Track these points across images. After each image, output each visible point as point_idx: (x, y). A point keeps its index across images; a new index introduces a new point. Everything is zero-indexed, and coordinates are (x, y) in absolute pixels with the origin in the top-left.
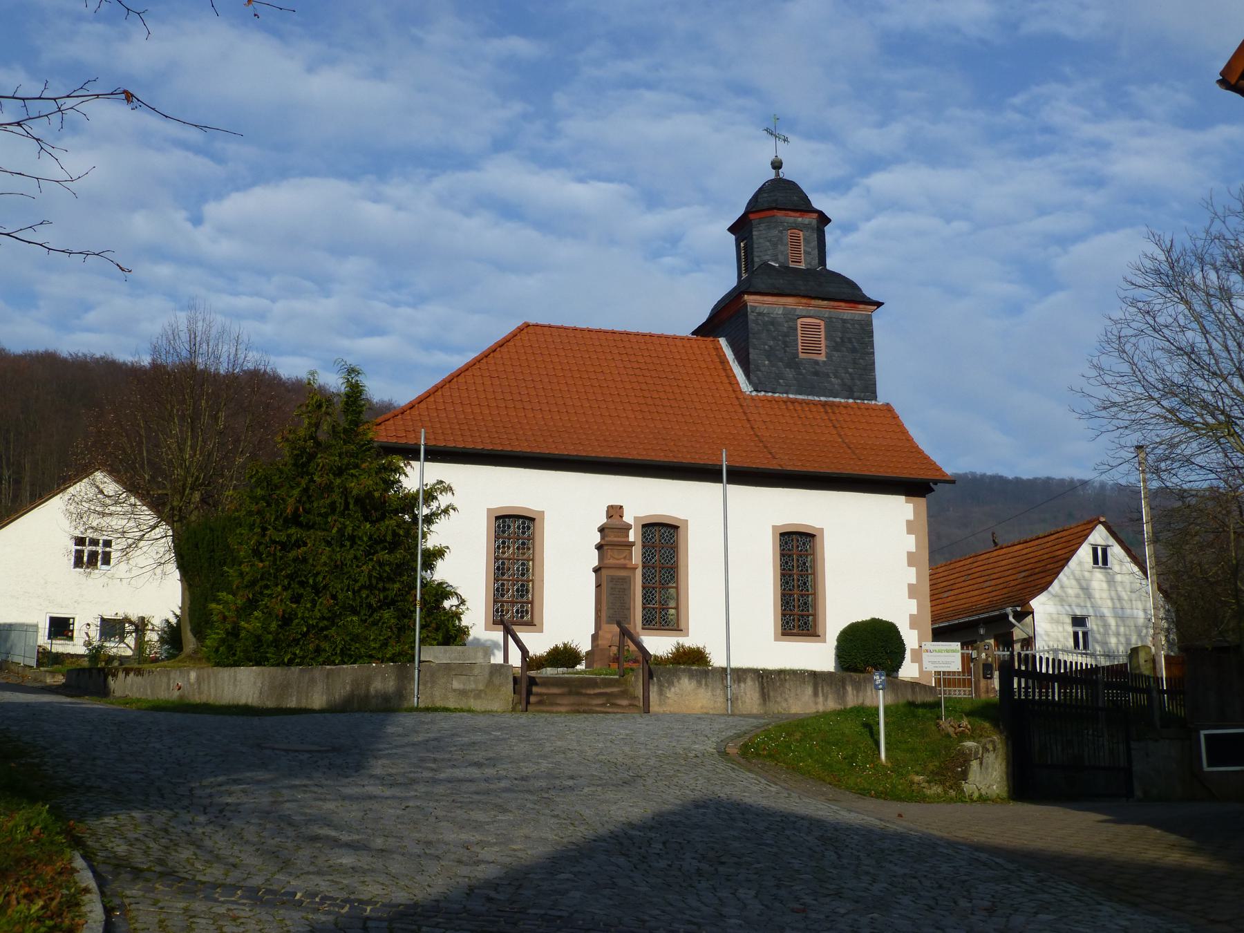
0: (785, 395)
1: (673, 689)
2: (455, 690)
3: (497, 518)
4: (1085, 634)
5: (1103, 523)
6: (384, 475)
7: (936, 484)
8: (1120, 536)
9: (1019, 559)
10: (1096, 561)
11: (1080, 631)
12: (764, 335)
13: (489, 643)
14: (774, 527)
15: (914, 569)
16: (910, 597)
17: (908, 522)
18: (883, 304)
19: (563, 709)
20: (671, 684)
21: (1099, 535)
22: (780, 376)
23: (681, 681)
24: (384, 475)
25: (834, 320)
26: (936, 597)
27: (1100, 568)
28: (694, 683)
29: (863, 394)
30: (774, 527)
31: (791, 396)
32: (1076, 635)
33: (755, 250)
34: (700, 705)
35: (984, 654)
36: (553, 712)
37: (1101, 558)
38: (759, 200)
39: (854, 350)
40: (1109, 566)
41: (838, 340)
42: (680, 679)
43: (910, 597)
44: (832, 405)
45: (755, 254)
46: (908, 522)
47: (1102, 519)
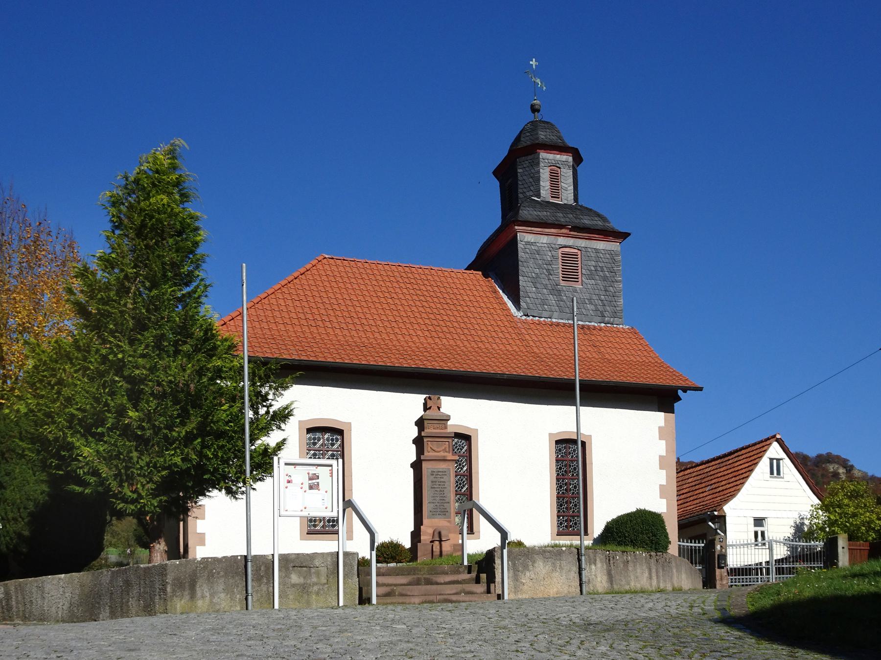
0: (549, 320)
1: (528, 574)
2: (294, 586)
3: (309, 431)
4: (763, 533)
5: (778, 440)
6: (106, 600)
7: (685, 390)
8: (336, 593)
9: (703, 476)
10: (772, 473)
11: (759, 529)
12: (531, 261)
13: (293, 556)
14: (550, 435)
15: (665, 471)
16: (661, 497)
17: (660, 428)
18: (628, 235)
19: (417, 600)
20: (526, 567)
21: (775, 451)
22: (544, 302)
23: (536, 565)
24: (106, 600)
25: (589, 250)
26: (683, 497)
27: (775, 477)
28: (549, 567)
29: (612, 319)
30: (550, 435)
31: (554, 320)
32: (756, 533)
33: (520, 186)
34: (555, 590)
35: (719, 546)
36: (405, 603)
37: (775, 469)
38: (522, 139)
39: (605, 279)
40: (782, 475)
41: (593, 268)
42: (534, 562)
43: (661, 497)
44: (589, 327)
45: (520, 190)
46: (660, 428)
47: (778, 436)
